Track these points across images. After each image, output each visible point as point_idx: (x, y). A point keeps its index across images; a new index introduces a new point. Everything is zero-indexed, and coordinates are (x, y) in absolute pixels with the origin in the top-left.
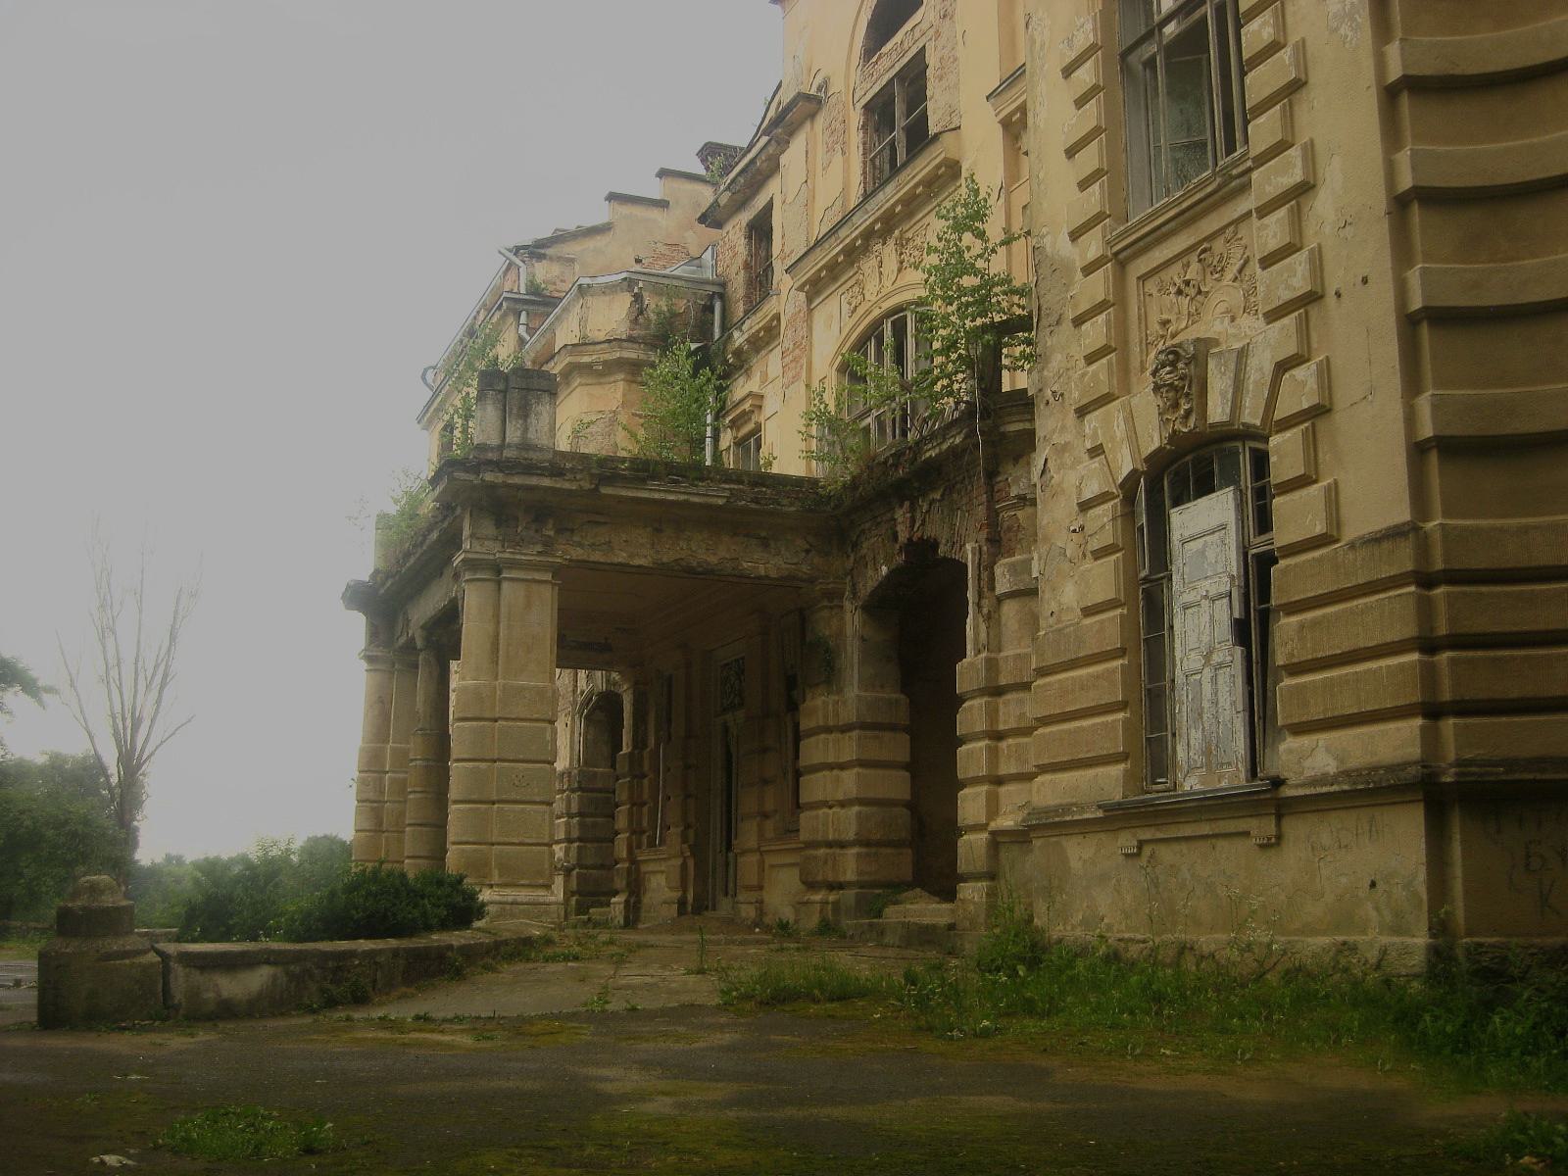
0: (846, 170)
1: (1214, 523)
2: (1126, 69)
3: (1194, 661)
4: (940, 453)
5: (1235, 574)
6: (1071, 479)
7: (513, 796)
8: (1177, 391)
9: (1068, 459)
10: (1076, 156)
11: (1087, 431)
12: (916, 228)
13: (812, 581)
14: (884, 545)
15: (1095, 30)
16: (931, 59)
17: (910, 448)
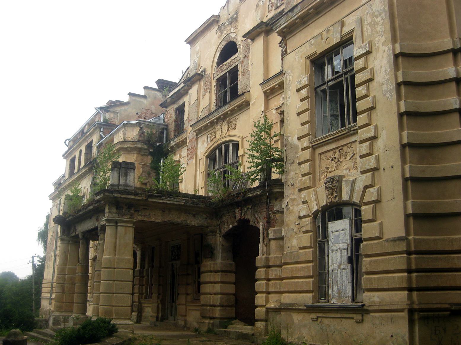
1: (343, 228)
2: (316, 92)
3: (335, 266)
4: (253, 196)
5: (349, 243)
6: (296, 209)
7: (120, 292)
8: (333, 190)
9: (295, 203)
10: (301, 115)
11: (302, 196)
12: (234, 119)
13: (207, 227)
14: (231, 219)
15: (308, 80)
16: (240, 69)
17: (243, 193)
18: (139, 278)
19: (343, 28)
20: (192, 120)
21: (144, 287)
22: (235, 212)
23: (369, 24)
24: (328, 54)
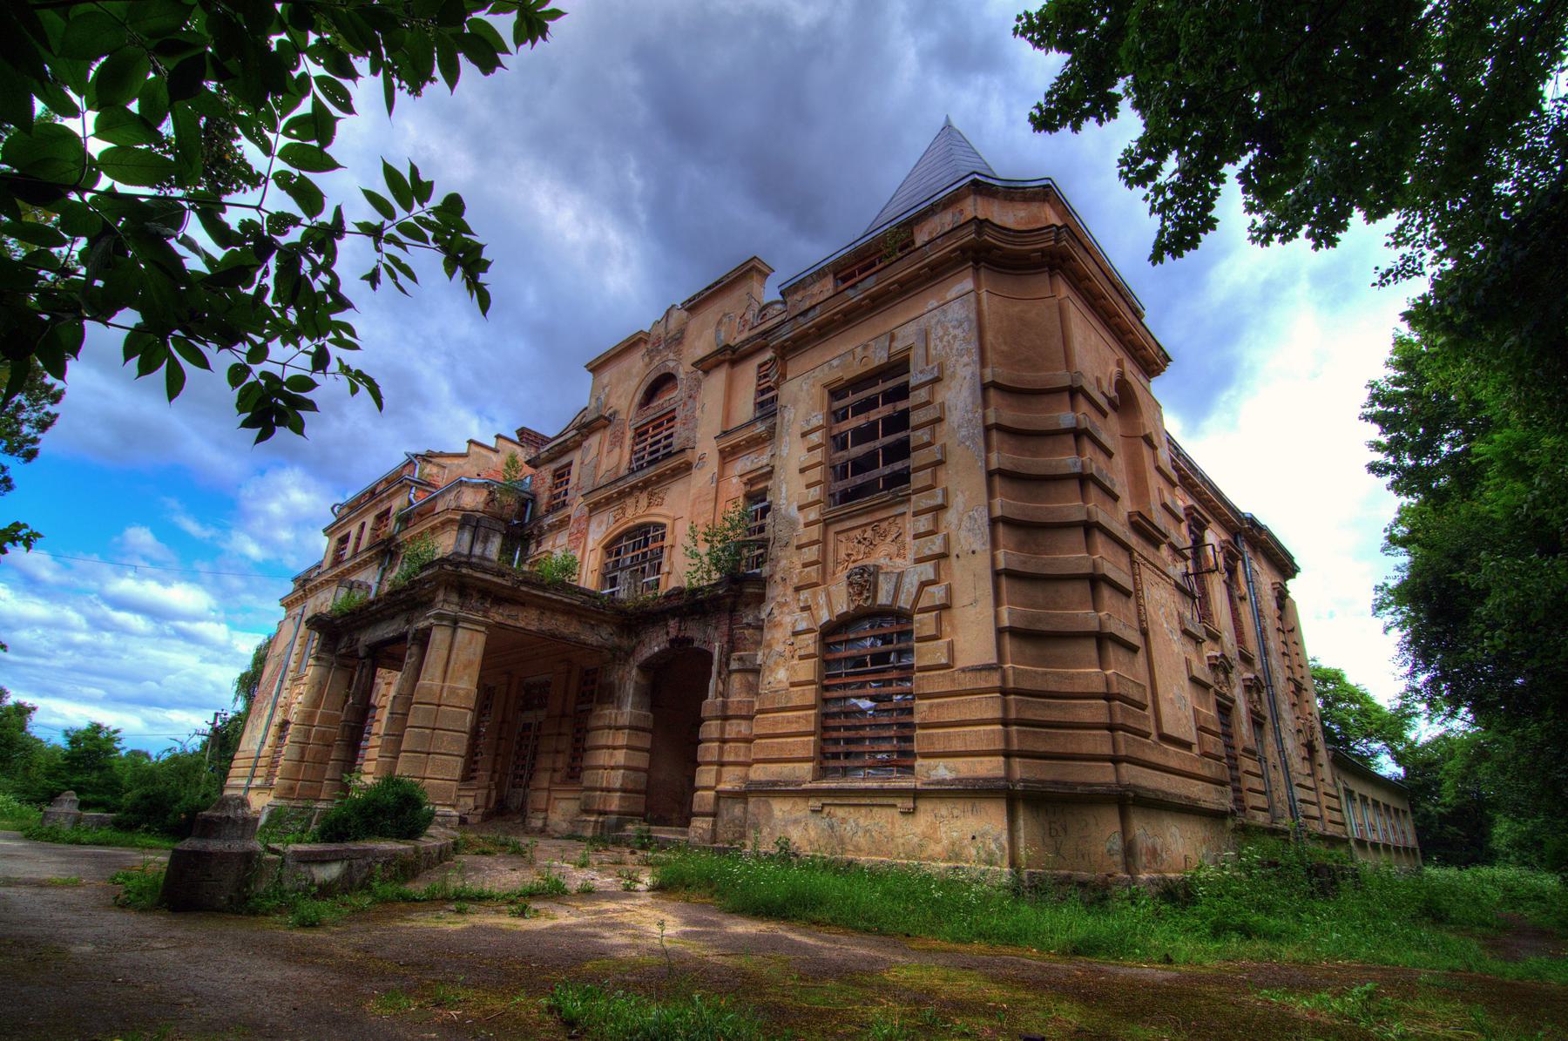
0: (621, 456)
6: (788, 619)
9: (785, 609)
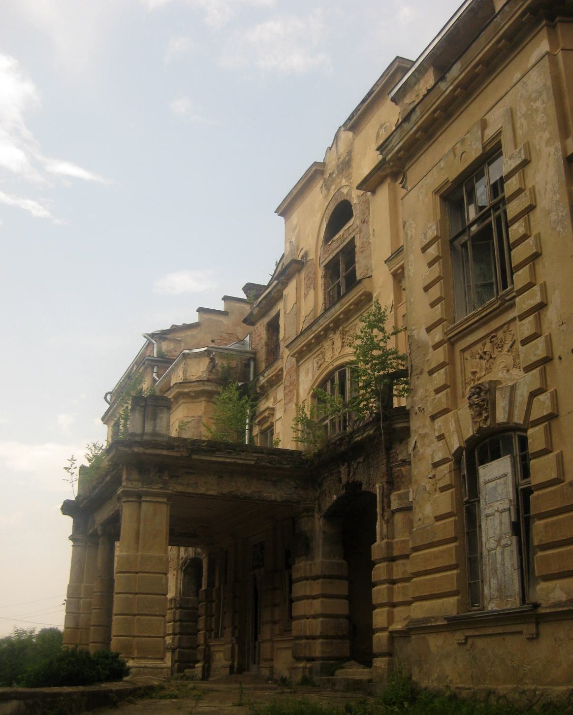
1: (501, 473)
3: (492, 544)
5: (512, 499)
6: (428, 451)
7: (146, 612)
9: (427, 441)
11: (436, 427)
12: (351, 326)
15: (437, 229)
16: (358, 243)
17: (348, 436)
18: (205, 603)
19: (485, 131)
20: (289, 337)
21: (213, 619)
22: (340, 472)
23: (523, 115)
24: (467, 181)
